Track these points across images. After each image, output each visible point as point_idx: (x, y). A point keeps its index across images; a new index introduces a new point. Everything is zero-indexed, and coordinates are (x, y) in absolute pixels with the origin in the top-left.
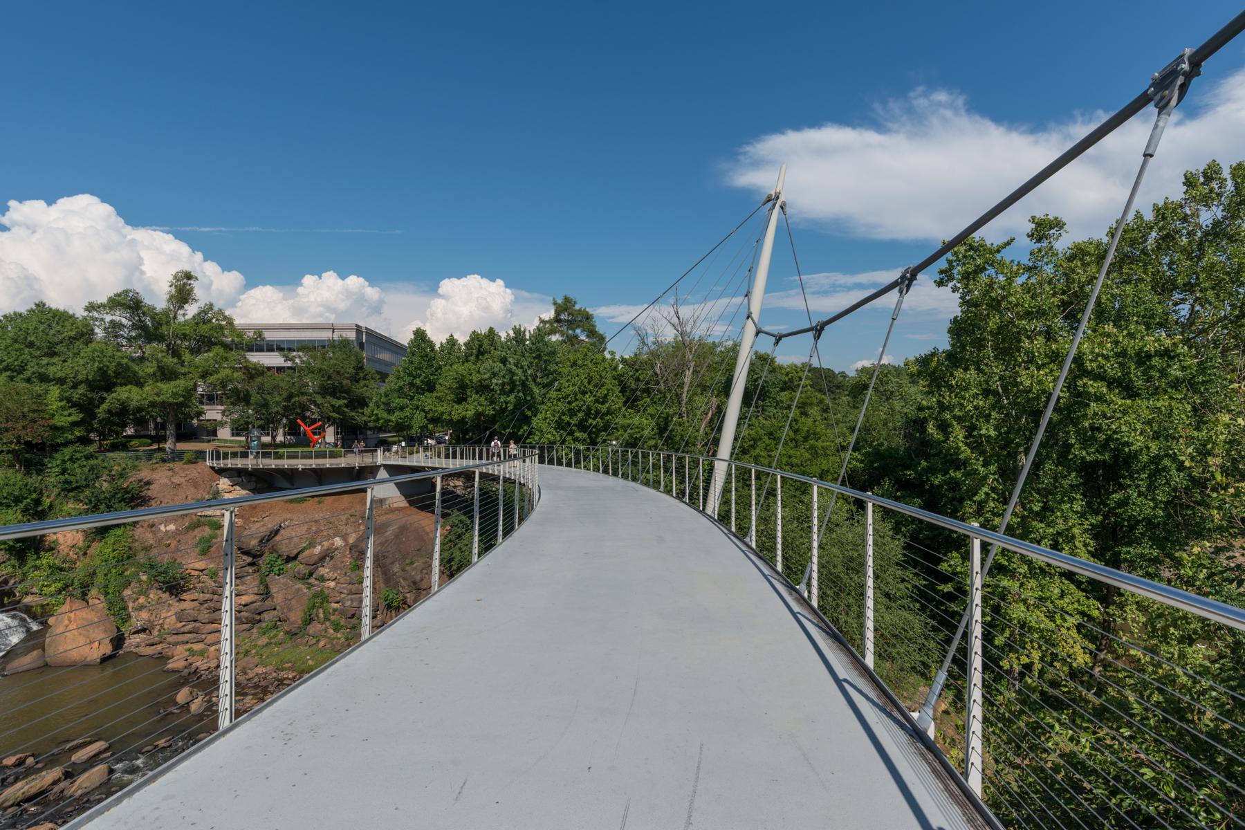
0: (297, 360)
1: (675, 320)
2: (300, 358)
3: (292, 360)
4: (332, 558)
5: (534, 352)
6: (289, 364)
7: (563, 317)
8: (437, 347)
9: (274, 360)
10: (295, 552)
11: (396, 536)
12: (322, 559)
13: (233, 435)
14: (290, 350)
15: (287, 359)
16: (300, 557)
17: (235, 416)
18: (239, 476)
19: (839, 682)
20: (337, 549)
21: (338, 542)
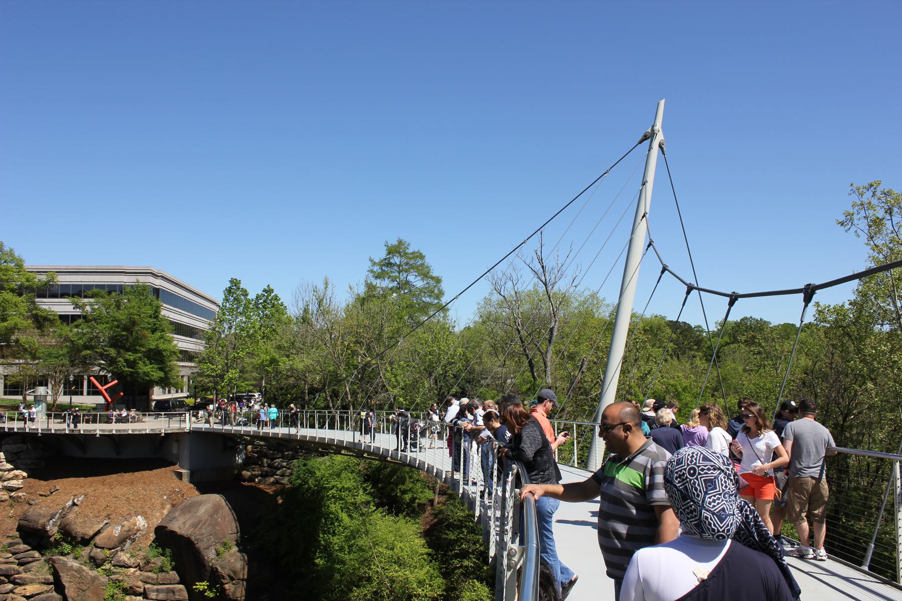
0: (88, 308)
1: (538, 267)
2: (89, 305)
3: (82, 307)
4: (134, 540)
5: (46, 284)
6: (78, 312)
7: (396, 260)
8: (252, 296)
9: (63, 307)
10: (91, 533)
11: (211, 516)
12: (122, 541)
13: (5, 393)
14: (79, 294)
15: (77, 306)
16: (98, 540)
17: (14, 370)
18: (24, 442)
19: (807, 573)
20: (138, 530)
21: (140, 521)
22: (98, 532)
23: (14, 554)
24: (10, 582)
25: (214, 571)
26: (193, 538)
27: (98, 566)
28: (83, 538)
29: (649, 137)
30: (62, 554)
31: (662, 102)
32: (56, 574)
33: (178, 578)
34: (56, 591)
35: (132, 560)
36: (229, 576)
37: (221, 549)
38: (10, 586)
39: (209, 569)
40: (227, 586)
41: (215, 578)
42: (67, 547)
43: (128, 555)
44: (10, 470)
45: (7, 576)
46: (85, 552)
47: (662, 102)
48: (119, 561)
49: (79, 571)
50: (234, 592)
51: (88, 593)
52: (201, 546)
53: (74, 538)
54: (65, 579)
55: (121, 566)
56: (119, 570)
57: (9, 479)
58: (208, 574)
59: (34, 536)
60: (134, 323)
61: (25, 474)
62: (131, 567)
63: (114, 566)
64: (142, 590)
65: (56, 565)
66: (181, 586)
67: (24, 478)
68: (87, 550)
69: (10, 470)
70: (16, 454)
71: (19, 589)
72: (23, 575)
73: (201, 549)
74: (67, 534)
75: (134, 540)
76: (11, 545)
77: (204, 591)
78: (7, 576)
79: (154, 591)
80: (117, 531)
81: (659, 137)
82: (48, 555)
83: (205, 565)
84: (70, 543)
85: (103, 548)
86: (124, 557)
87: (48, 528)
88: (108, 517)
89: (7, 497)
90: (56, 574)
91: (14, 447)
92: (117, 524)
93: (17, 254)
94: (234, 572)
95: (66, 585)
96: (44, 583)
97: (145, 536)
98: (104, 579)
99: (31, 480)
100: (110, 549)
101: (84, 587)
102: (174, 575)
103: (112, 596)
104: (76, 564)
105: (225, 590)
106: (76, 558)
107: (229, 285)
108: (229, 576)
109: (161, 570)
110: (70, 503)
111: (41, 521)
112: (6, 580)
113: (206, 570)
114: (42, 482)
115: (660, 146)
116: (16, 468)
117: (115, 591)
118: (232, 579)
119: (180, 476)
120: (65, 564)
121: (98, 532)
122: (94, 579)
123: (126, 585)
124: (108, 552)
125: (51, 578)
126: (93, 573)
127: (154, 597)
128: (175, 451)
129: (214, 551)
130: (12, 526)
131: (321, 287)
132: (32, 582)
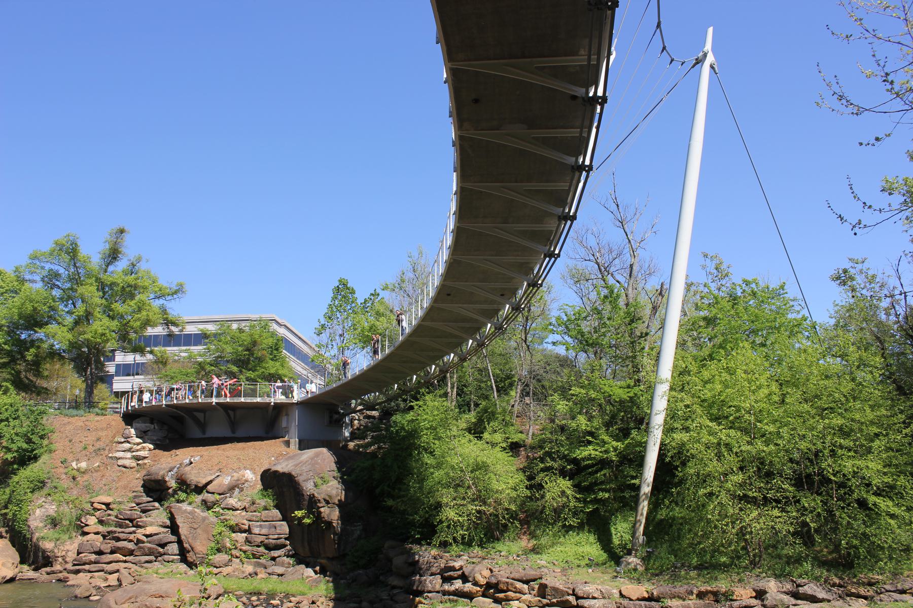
4: (242, 490)
10: (204, 481)
12: (231, 489)
22: (211, 482)
23: (138, 504)
24: (133, 526)
25: (312, 498)
26: (293, 473)
27: (209, 508)
28: (196, 486)
29: (699, 62)
30: (178, 501)
31: (710, 30)
32: (172, 518)
33: (280, 516)
34: (172, 534)
35: (239, 504)
36: (325, 500)
37: (319, 481)
38: (134, 529)
39: (307, 498)
40: (322, 510)
41: (312, 504)
42: (183, 496)
43: (236, 500)
44: (138, 444)
45: (131, 520)
46: (198, 499)
47: (710, 30)
48: (227, 504)
49: (192, 513)
50: (329, 515)
51: (199, 531)
52: (300, 479)
53: (188, 486)
54: (179, 521)
55: (229, 509)
56: (227, 512)
57: (137, 451)
58: (306, 503)
59: (156, 489)
60: (254, 343)
61: (151, 446)
62: (237, 510)
63: (223, 509)
64: (247, 527)
65: (173, 510)
66: (284, 523)
67: (150, 450)
68: (200, 497)
69: (138, 444)
70: (145, 432)
71: (140, 530)
72: (145, 519)
73: (301, 481)
74: (183, 484)
75: (242, 490)
76: (135, 497)
77: (303, 517)
78: (131, 520)
79: (257, 526)
80: (226, 480)
81: (710, 59)
82: (166, 504)
83: (303, 495)
84: (185, 492)
85: (213, 493)
86: (232, 502)
87: (167, 479)
88: (220, 470)
89: (134, 464)
90: (172, 518)
91: (143, 426)
92: (227, 475)
93: (152, 274)
94: (330, 496)
95: (180, 525)
96: (162, 526)
97: (253, 487)
98: (213, 519)
99: (157, 451)
100: (220, 494)
101: (196, 526)
102: (276, 513)
103: (220, 534)
104: (189, 508)
105: (321, 513)
106: (190, 504)
107: (337, 284)
108: (325, 500)
109: (266, 509)
110: (187, 461)
111: (161, 473)
112: (131, 524)
113: (304, 500)
114: (166, 453)
115: (712, 67)
116: (144, 442)
117: (223, 529)
118: (327, 502)
119: (287, 444)
120: (180, 508)
121: (211, 482)
122: (204, 519)
123: (232, 523)
124: (218, 497)
125: (168, 523)
126: (205, 514)
127: (257, 532)
128: (284, 424)
129: (312, 484)
130: (138, 485)
131: (415, 254)
132: (152, 524)
